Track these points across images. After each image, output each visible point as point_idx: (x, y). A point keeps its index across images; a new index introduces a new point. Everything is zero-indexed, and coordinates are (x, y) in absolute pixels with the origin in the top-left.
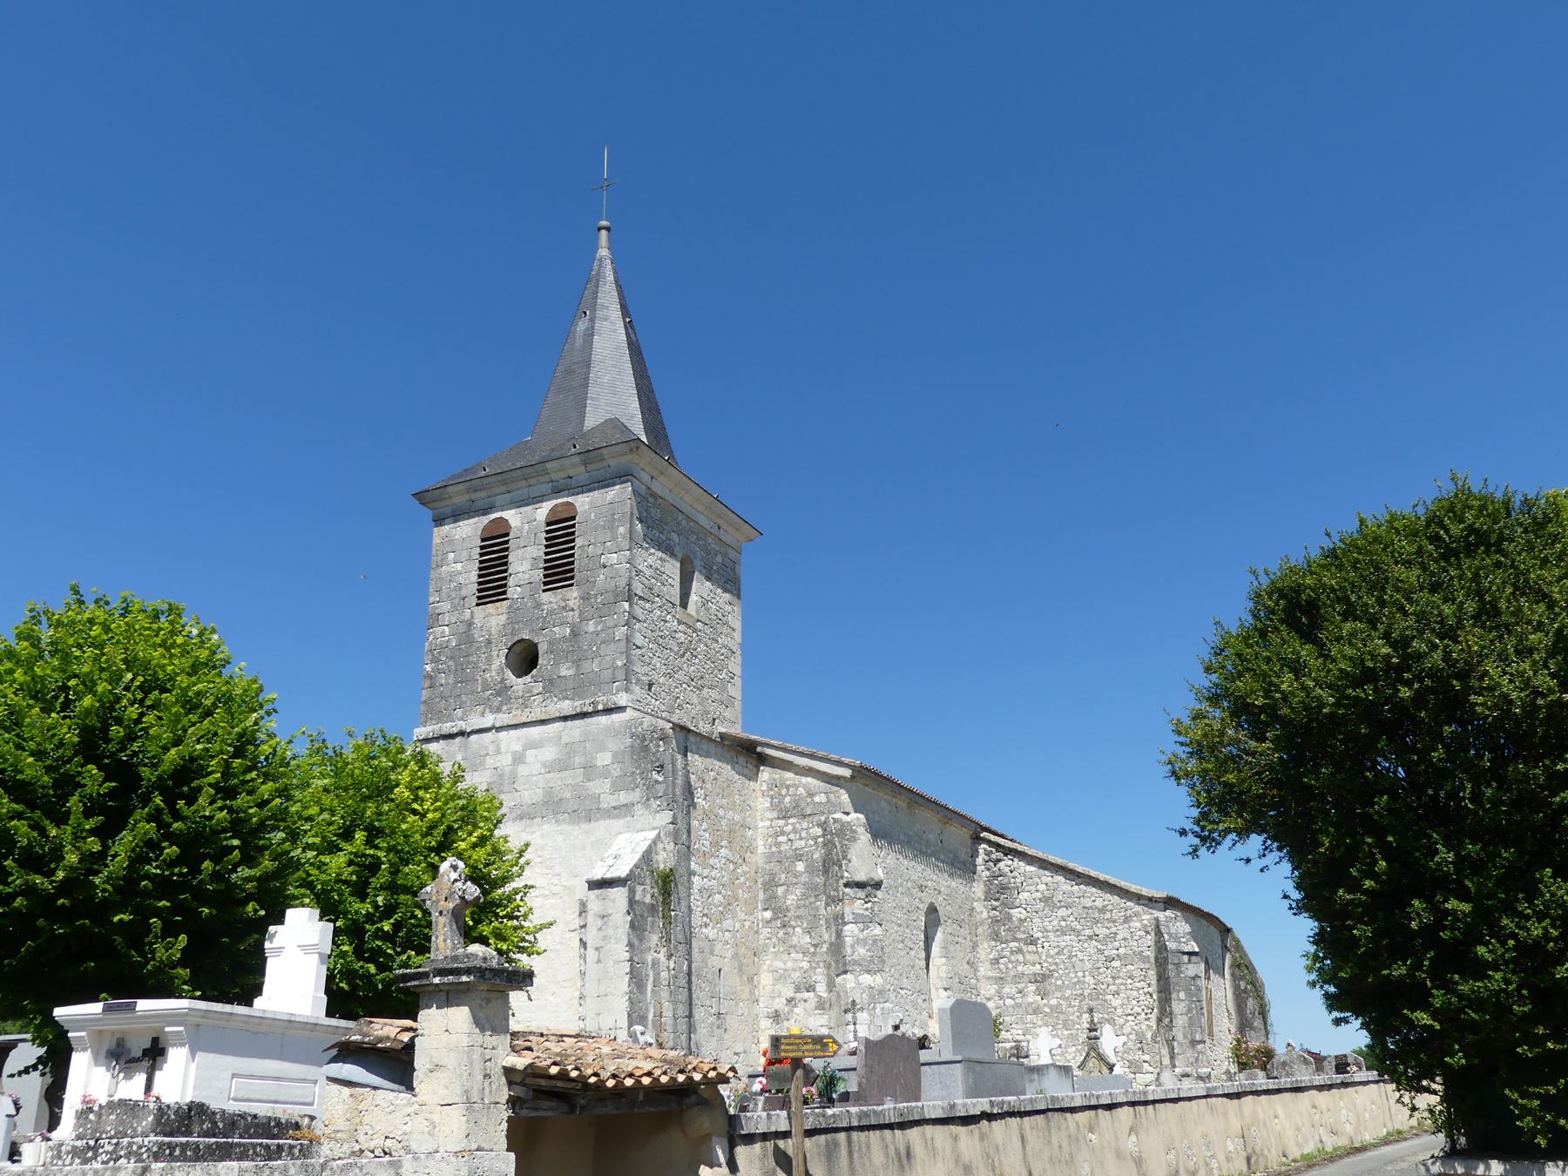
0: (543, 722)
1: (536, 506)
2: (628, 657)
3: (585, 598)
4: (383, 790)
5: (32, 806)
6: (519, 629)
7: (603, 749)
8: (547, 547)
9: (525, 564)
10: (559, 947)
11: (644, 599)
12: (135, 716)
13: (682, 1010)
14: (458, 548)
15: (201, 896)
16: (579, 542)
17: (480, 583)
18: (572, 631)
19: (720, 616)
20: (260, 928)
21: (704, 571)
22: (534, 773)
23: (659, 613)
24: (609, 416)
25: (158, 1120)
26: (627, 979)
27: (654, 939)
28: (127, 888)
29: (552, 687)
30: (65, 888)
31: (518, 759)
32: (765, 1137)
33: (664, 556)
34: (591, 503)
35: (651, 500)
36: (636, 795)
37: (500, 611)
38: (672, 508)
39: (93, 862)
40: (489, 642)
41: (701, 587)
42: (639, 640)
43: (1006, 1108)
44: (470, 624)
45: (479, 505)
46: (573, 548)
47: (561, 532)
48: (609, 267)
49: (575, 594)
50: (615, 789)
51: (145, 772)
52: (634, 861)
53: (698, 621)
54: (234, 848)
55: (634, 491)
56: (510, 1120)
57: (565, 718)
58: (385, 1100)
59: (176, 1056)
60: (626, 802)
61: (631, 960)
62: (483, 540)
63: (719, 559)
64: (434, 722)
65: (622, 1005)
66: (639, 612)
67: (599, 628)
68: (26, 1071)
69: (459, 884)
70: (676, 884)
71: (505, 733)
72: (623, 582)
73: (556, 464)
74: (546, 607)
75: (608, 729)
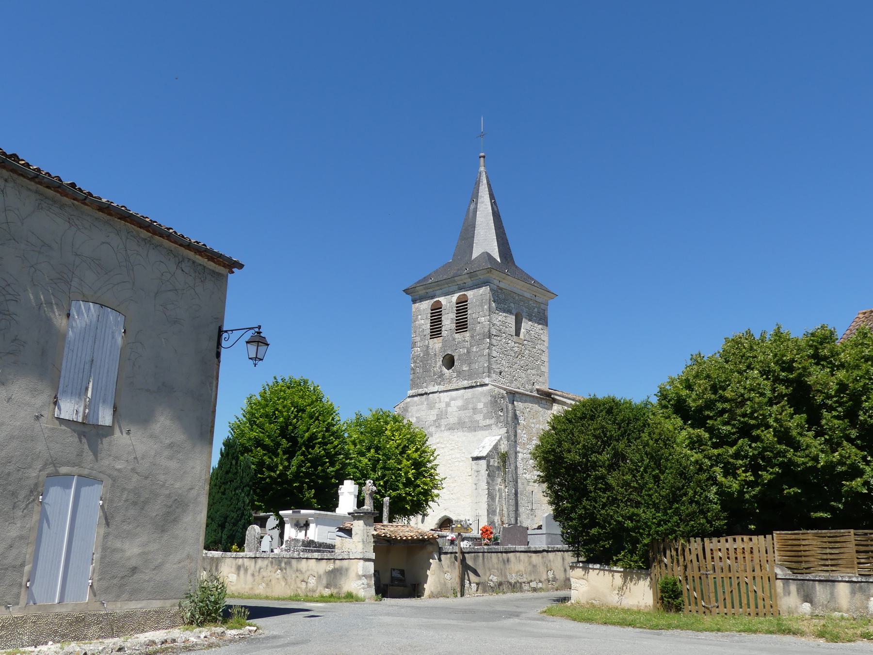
0: (457, 390)
1: (452, 295)
2: (489, 362)
3: (472, 337)
4: (380, 432)
5: (269, 452)
6: (447, 350)
7: (480, 402)
8: (457, 314)
9: (448, 321)
10: (465, 482)
11: (497, 336)
12: (295, 422)
13: (512, 508)
14: (422, 313)
15: (318, 477)
16: (469, 312)
17: (431, 329)
18: (467, 351)
19: (536, 336)
20: (337, 486)
21: (528, 317)
22: (454, 411)
23: (504, 340)
24: (483, 251)
25: (303, 543)
26: (487, 496)
27: (499, 480)
28: (297, 476)
29: (460, 374)
30: (280, 476)
31: (448, 405)
32: (451, 553)
33: (506, 315)
34: (474, 294)
35: (499, 291)
36: (492, 421)
37: (439, 341)
38: (510, 292)
39: (287, 468)
40: (435, 355)
41: (526, 325)
42: (494, 354)
43: (555, 549)
44: (428, 347)
45: (429, 295)
46: (467, 314)
47: (462, 307)
48: (484, 176)
49: (468, 335)
50: (485, 418)
51: (299, 439)
52: (490, 449)
53: (524, 341)
54: (327, 462)
55: (490, 289)
56: (374, 546)
57: (465, 388)
58: (348, 540)
59: (312, 526)
60: (489, 424)
61: (488, 489)
62: (432, 310)
63: (536, 310)
64: (415, 388)
65: (485, 506)
66: (494, 342)
67: (478, 350)
68: (273, 528)
69: (371, 487)
70: (508, 458)
71: (442, 394)
72: (486, 330)
73: (459, 278)
74: (457, 340)
75: (482, 393)
